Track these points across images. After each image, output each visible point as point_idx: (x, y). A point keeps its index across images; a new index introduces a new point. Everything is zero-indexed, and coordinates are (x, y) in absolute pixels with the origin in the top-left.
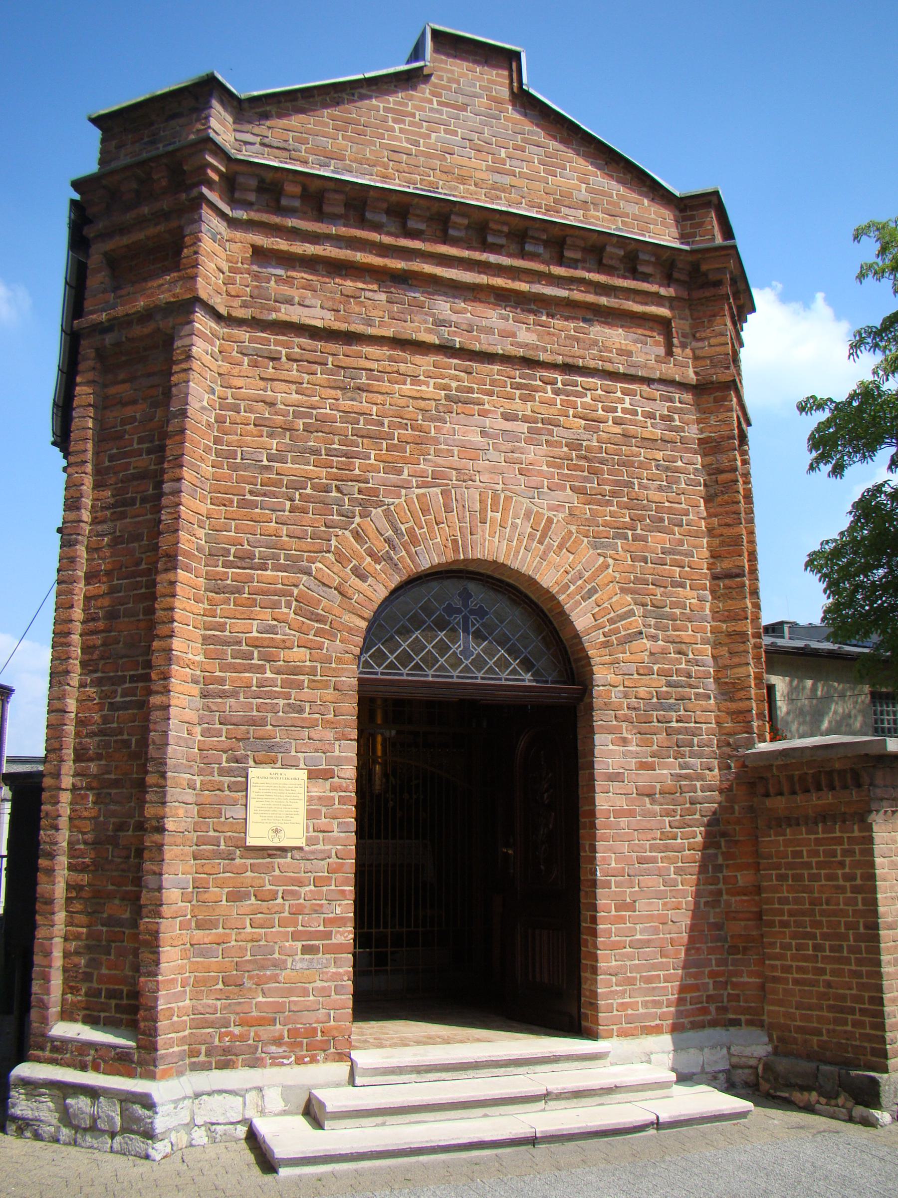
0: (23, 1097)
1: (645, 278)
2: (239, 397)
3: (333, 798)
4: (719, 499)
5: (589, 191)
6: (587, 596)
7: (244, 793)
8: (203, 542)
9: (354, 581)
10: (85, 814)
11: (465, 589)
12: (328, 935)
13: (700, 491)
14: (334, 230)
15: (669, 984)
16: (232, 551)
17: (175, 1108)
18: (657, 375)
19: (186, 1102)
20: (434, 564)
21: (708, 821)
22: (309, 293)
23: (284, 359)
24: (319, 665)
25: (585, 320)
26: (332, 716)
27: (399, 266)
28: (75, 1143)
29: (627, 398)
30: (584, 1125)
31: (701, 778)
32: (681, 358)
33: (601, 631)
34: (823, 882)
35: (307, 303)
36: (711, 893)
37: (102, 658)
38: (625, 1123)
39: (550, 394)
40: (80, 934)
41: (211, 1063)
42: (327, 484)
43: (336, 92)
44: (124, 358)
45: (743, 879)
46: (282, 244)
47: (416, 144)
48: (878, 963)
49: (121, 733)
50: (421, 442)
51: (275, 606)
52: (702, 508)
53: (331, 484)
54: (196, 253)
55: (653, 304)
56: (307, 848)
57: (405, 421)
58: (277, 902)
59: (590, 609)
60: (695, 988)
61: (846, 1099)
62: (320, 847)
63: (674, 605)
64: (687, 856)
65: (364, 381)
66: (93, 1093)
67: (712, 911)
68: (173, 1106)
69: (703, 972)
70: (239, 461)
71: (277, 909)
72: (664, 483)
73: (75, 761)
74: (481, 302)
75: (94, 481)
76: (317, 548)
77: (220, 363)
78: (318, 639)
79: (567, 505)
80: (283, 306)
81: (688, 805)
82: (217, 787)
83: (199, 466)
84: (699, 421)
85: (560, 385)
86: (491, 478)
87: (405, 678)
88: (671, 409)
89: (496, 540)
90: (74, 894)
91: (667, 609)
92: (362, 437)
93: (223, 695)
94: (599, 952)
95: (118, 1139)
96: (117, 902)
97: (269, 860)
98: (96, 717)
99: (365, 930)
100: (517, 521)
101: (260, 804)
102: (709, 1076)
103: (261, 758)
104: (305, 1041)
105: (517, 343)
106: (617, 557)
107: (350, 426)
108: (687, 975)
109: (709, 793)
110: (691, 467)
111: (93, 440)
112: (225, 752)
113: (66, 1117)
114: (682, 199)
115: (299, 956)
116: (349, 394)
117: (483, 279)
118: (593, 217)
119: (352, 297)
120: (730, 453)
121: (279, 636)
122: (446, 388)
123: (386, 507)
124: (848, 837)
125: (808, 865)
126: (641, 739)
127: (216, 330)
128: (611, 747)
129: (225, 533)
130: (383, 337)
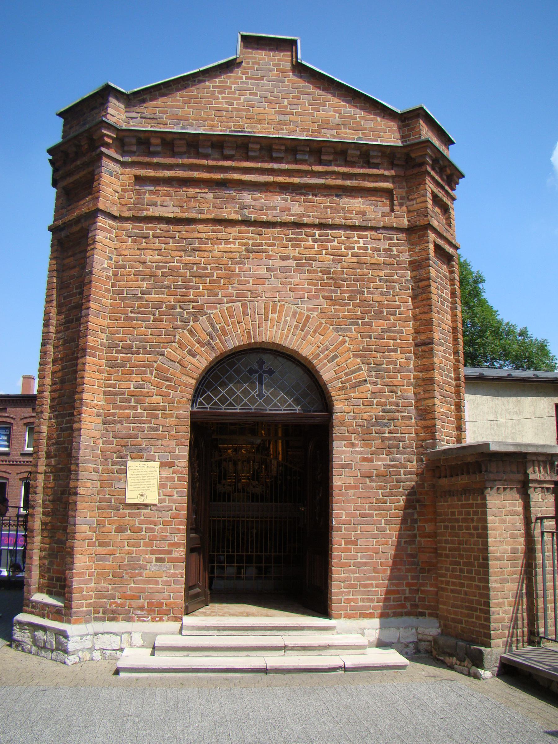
0: (18, 630)
1: (376, 166)
2: (125, 260)
3: (174, 477)
4: (420, 297)
6: (331, 360)
8: (105, 341)
9: (189, 357)
10: (50, 486)
11: (261, 359)
12: (170, 552)
13: (409, 293)
14: (180, 161)
15: (379, 589)
16: (121, 345)
17: (81, 639)
18: (382, 224)
19: (89, 637)
20: (236, 346)
21: (408, 492)
22: (168, 198)
23: (151, 237)
24: (167, 405)
25: (337, 196)
26: (174, 433)
27: (219, 177)
28: (37, 654)
29: (361, 241)
30: (297, 664)
31: (405, 467)
32: (399, 213)
33: (339, 380)
34: (464, 531)
35: (165, 204)
36: (409, 536)
37: (58, 404)
38: (323, 666)
39: (311, 242)
40: (46, 548)
41: (105, 618)
42: (174, 305)
43: (184, 81)
44: (71, 244)
45: (429, 528)
46: (151, 173)
47: (232, 104)
48: (487, 581)
49: (64, 443)
50: (230, 277)
51: (144, 373)
52: (410, 303)
53: (176, 305)
54: (99, 184)
55: (381, 181)
56: (159, 505)
57: (221, 266)
58: (142, 533)
59: (333, 367)
60: (397, 592)
61: (468, 662)
63: (388, 363)
64: (393, 513)
65: (197, 245)
66: (44, 629)
67: (409, 547)
68: (79, 638)
69: (403, 583)
70: (125, 295)
71: (142, 537)
72: (385, 290)
73: (46, 458)
74: (270, 192)
75: (57, 310)
76: (168, 340)
77: (116, 242)
78: (167, 390)
79: (319, 307)
80: (151, 207)
81: (395, 483)
82: (110, 472)
83: (101, 300)
84: (409, 250)
85: (317, 236)
86: (272, 295)
87: (208, 410)
88: (391, 245)
89: (274, 330)
90: (44, 528)
91: (384, 366)
92: (195, 277)
93: (114, 422)
94: (333, 568)
95: (54, 653)
96: (61, 531)
97: (138, 511)
98: (55, 435)
99: (278, 554)
100: (287, 318)
101: (133, 481)
102: (403, 645)
103: (134, 456)
104: (157, 609)
105: (291, 214)
107: (188, 271)
108: (392, 584)
109: (409, 476)
110: (403, 279)
111: (57, 289)
112: (115, 453)
113: (35, 642)
114: (402, 114)
115: (154, 563)
116: (188, 253)
117: (271, 179)
118: (343, 133)
119: (193, 198)
120: (426, 269)
121: (145, 390)
124: (476, 503)
125: (457, 520)
126: (364, 444)
127: (113, 225)
128: (344, 448)
130: (208, 219)
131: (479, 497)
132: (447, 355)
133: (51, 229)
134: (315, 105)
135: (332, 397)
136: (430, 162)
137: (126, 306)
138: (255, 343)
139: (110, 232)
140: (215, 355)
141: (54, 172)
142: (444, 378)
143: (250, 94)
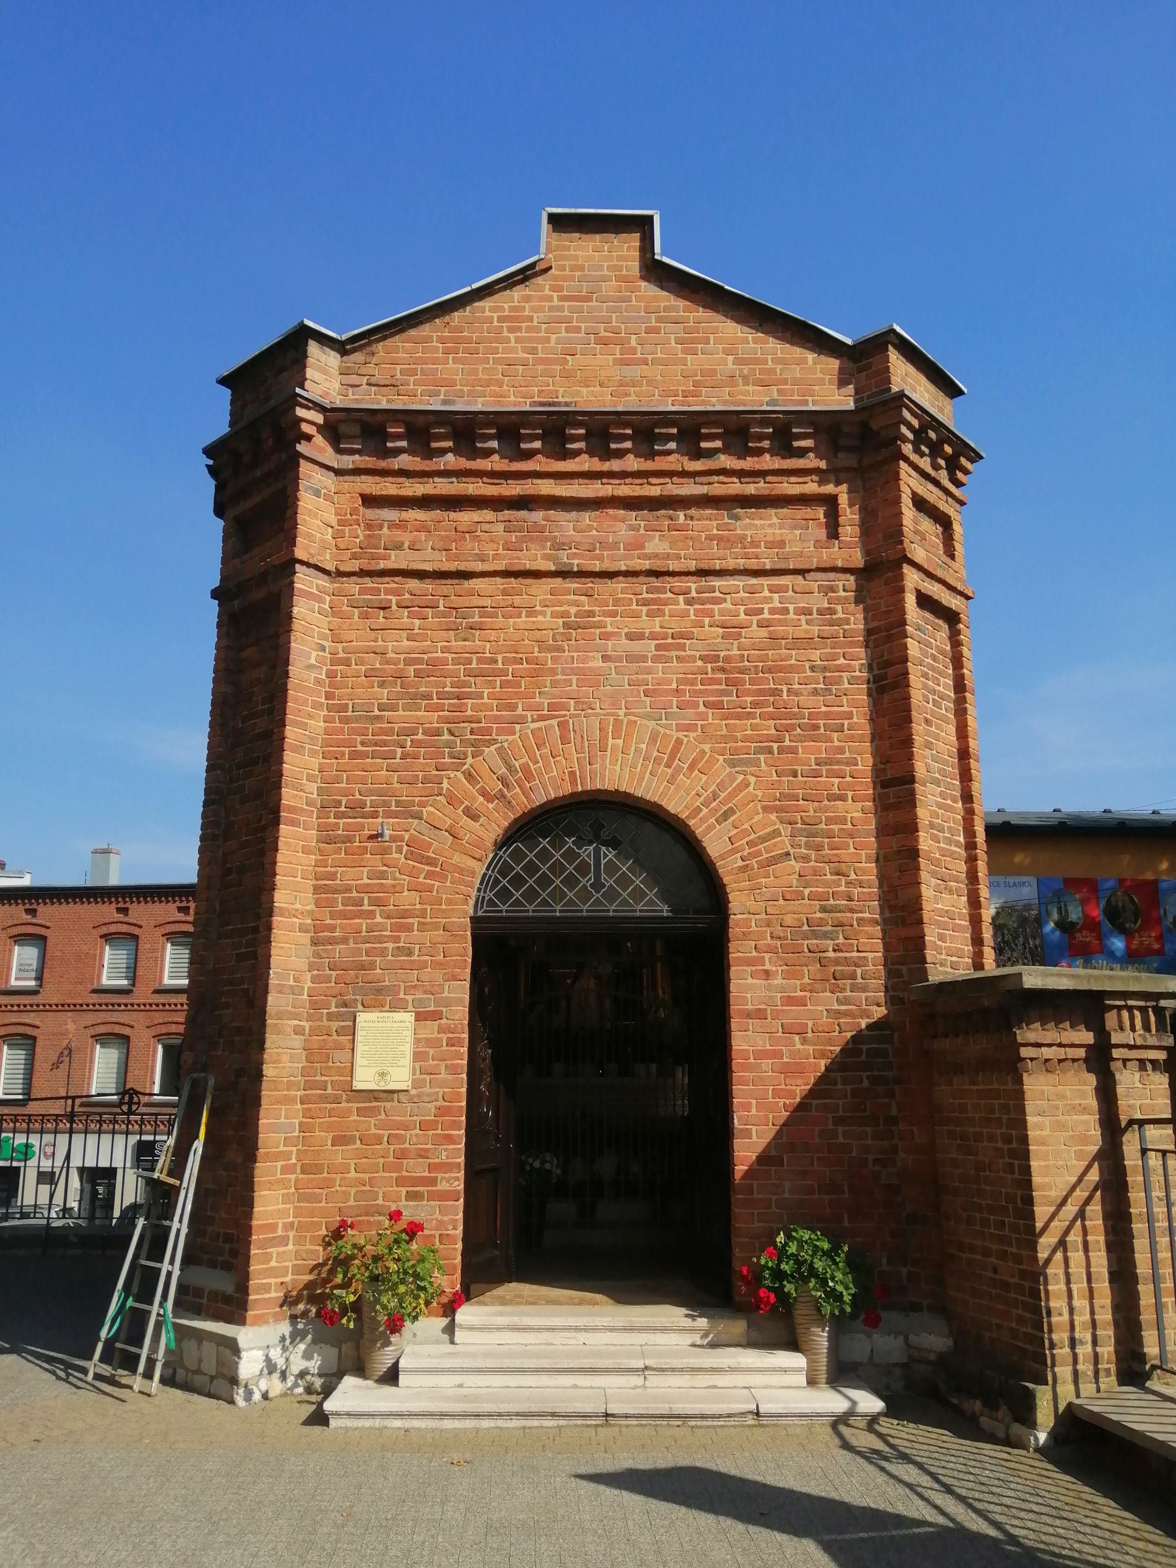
3: (440, 1040)
5: (739, 362)
7: (351, 1037)
8: (315, 796)
9: (466, 820)
12: (432, 1182)
20: (550, 799)
26: (441, 957)
29: (776, 596)
33: (739, 854)
39: (682, 606)
42: (438, 728)
47: (534, 351)
53: (442, 728)
57: (521, 655)
62: (427, 1090)
63: (829, 821)
65: (477, 619)
77: (331, 619)
78: (429, 881)
82: (325, 1032)
83: (307, 724)
85: (694, 594)
88: (833, 601)
89: (618, 768)
93: (332, 941)
101: (366, 1048)
106: (758, 774)
107: (462, 667)
121: (389, 881)
122: (565, 615)
123: (500, 745)
127: (324, 587)
128: (750, 981)
129: (336, 785)
131: (1009, 1078)
132: (949, 802)
133: (215, 594)
134: (689, 343)
135: (725, 885)
136: (910, 436)
137: (353, 731)
138: (584, 792)
139: (320, 600)
140: (513, 817)
141: (219, 489)
142: (942, 845)
143: (568, 330)
